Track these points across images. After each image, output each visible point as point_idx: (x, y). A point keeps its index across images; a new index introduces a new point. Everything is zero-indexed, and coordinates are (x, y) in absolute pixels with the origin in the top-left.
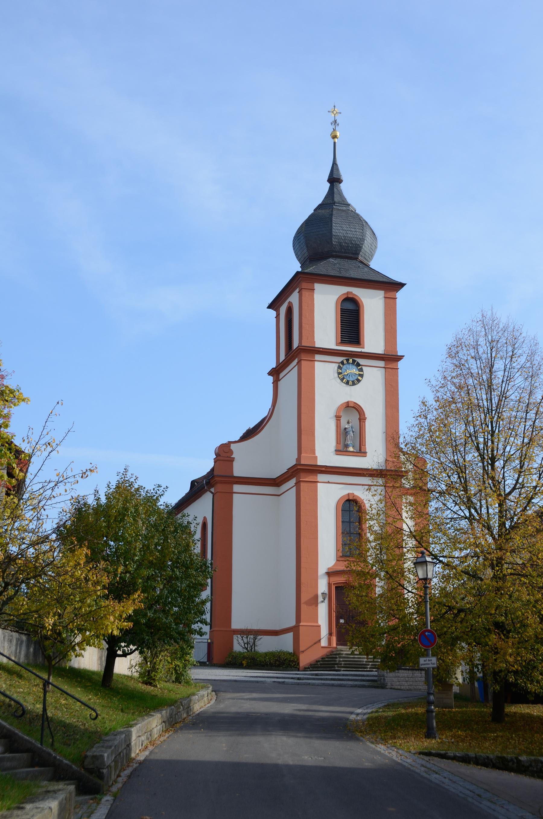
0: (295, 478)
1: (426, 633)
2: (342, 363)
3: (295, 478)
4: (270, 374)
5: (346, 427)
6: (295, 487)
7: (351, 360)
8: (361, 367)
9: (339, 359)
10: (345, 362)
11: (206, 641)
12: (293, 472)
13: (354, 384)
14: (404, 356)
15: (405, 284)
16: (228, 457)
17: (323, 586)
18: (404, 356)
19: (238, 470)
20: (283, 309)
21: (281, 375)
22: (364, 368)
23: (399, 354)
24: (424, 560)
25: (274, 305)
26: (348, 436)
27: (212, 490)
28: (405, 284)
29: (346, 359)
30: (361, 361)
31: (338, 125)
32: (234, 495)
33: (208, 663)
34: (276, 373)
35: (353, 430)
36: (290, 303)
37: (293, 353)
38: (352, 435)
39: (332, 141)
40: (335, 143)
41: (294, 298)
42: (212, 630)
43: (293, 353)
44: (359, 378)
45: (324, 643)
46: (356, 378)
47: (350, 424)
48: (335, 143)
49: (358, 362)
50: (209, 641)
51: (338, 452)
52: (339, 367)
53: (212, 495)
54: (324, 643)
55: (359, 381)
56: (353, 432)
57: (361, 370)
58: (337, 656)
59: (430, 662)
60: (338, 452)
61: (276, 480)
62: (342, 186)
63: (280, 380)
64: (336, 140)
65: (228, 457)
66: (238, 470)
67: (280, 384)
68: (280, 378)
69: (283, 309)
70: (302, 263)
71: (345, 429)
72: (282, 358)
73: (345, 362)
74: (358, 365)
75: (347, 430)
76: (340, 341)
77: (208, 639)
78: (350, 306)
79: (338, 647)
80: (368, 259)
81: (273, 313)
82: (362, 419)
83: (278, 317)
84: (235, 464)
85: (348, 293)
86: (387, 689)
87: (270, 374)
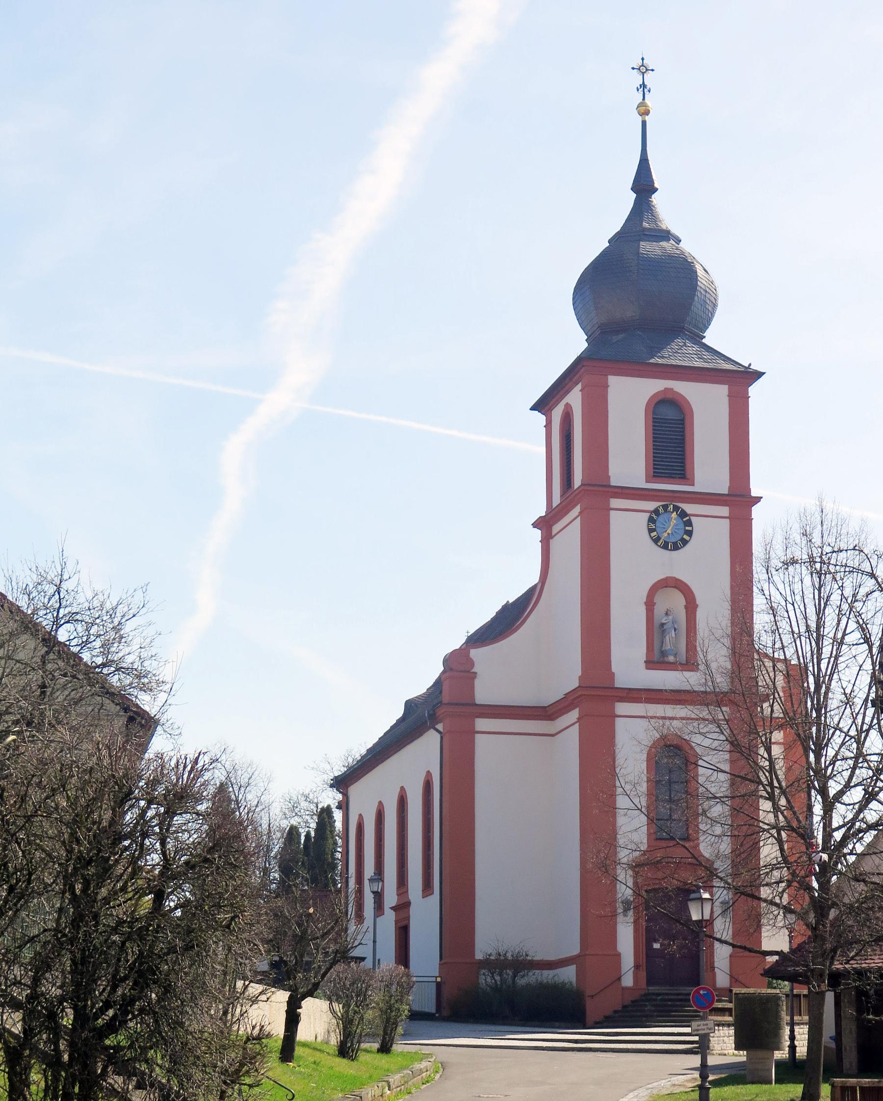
0: (577, 710)
1: (701, 992)
2: (656, 511)
3: (578, 709)
4: (535, 525)
5: (663, 621)
6: (578, 724)
7: (672, 506)
8: (688, 518)
9: (652, 505)
10: (661, 510)
11: (434, 979)
12: (574, 699)
13: (676, 547)
14: (762, 498)
15: (764, 373)
16: (465, 671)
17: (625, 891)
18: (762, 498)
19: (484, 694)
20: (557, 413)
21: (556, 528)
22: (693, 519)
23: (754, 493)
24: (699, 896)
25: (543, 405)
26: (667, 637)
27: (440, 727)
28: (764, 373)
29: (663, 506)
30: (689, 508)
31: (649, 91)
32: (477, 736)
33: (437, 1015)
34: (545, 524)
35: (676, 626)
36: (568, 407)
37: (572, 496)
38: (674, 636)
39: (640, 119)
40: (644, 123)
41: (575, 398)
42: (443, 961)
43: (572, 496)
44: (686, 537)
45: (628, 981)
46: (679, 537)
47: (670, 617)
48: (644, 123)
49: (683, 511)
50: (439, 979)
51: (652, 663)
52: (651, 520)
53: (438, 736)
54: (628, 981)
55: (685, 542)
56: (675, 630)
57: (689, 523)
58: (647, 1003)
59: (705, 1027)
60: (652, 663)
61: (547, 709)
62: (656, 199)
63: (552, 537)
64: (647, 118)
65: (465, 671)
66: (484, 694)
67: (554, 543)
68: (554, 532)
69: (557, 413)
70: (589, 334)
71: (662, 625)
72: (557, 500)
73: (661, 510)
74: (683, 514)
75: (665, 627)
76: (652, 474)
77: (436, 977)
78: (669, 413)
79: (649, 988)
80: (701, 326)
81: (540, 419)
82: (691, 606)
83: (548, 426)
84: (477, 682)
85: (667, 390)
86: (713, 1054)
87: (535, 525)
